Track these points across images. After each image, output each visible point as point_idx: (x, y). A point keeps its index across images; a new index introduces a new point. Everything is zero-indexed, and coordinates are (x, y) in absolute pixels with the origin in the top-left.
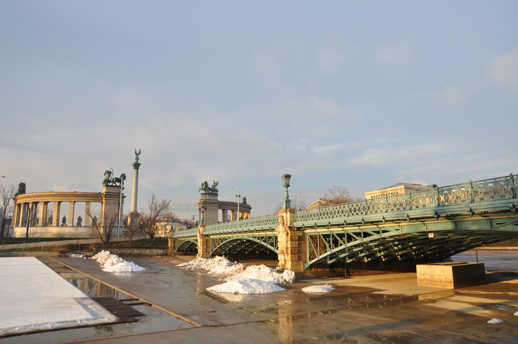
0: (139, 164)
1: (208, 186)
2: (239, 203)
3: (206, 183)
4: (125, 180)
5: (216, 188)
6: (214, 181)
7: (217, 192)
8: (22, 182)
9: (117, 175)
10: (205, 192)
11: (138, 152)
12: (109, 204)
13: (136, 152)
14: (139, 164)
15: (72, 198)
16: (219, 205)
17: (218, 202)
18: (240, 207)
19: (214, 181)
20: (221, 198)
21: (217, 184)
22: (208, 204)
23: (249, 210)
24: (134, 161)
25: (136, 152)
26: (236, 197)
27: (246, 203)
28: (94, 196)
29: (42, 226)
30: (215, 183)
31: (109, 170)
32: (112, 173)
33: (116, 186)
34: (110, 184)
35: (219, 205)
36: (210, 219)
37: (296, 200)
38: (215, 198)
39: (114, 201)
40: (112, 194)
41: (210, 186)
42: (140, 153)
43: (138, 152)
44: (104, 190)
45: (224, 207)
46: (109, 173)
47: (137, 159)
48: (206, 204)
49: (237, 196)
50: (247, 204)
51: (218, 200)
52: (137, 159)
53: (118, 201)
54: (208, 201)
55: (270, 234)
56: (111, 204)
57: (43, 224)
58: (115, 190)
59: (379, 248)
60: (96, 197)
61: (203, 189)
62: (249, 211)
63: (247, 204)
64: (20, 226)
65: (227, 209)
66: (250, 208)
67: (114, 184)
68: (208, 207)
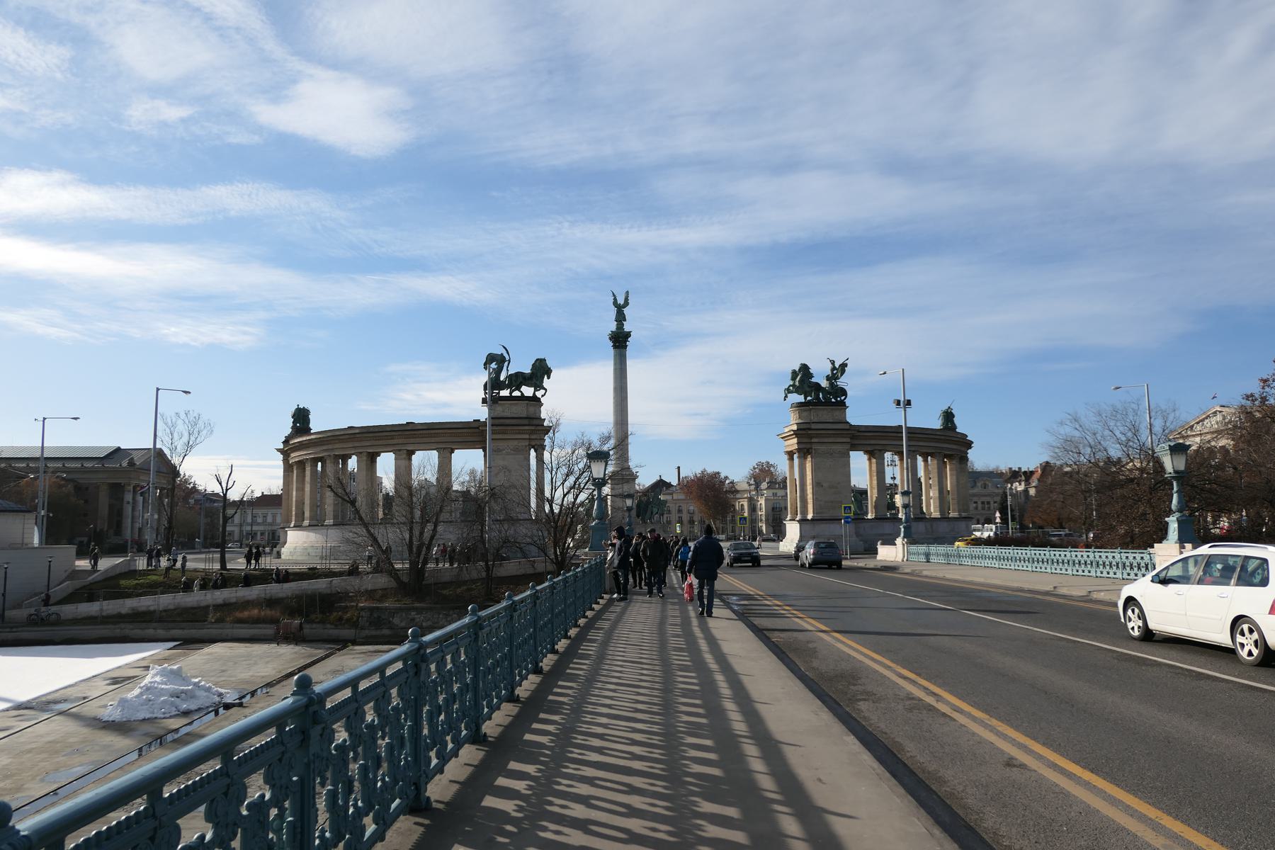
0: (628, 335)
1: (813, 380)
2: (908, 428)
3: (805, 368)
4: (549, 378)
5: (841, 382)
6: (833, 362)
7: (843, 398)
8: (301, 406)
9: (521, 364)
10: (805, 399)
11: (621, 301)
12: (500, 453)
13: (615, 299)
14: (628, 335)
15: (401, 441)
16: (853, 437)
17: (848, 427)
18: (909, 439)
19: (833, 362)
20: (856, 415)
21: (843, 372)
22: (817, 436)
23: (963, 449)
24: (613, 326)
25: (615, 299)
26: (894, 406)
27: (954, 427)
28: (459, 431)
29: (334, 525)
30: (834, 368)
31: (499, 351)
32: (507, 358)
33: (523, 398)
34: (505, 393)
35: (851, 438)
36: (824, 485)
37: (1134, 406)
38: (837, 414)
39: (516, 443)
40: (508, 422)
41: (820, 375)
42: (626, 303)
43: (621, 301)
44: (483, 413)
45: (873, 442)
46: (496, 361)
47: (620, 318)
48: (810, 437)
49: (898, 403)
50: (957, 430)
51: (848, 422)
52: (620, 318)
53: (527, 444)
54: (813, 426)
55: (271, 534)
56: (508, 454)
57: (335, 517)
58: (519, 410)
59: (318, 837)
60: (466, 434)
61: (798, 390)
62: (961, 451)
63: (957, 430)
64: (306, 523)
65: (880, 450)
66: (969, 445)
67: (516, 393)
68: (814, 447)
